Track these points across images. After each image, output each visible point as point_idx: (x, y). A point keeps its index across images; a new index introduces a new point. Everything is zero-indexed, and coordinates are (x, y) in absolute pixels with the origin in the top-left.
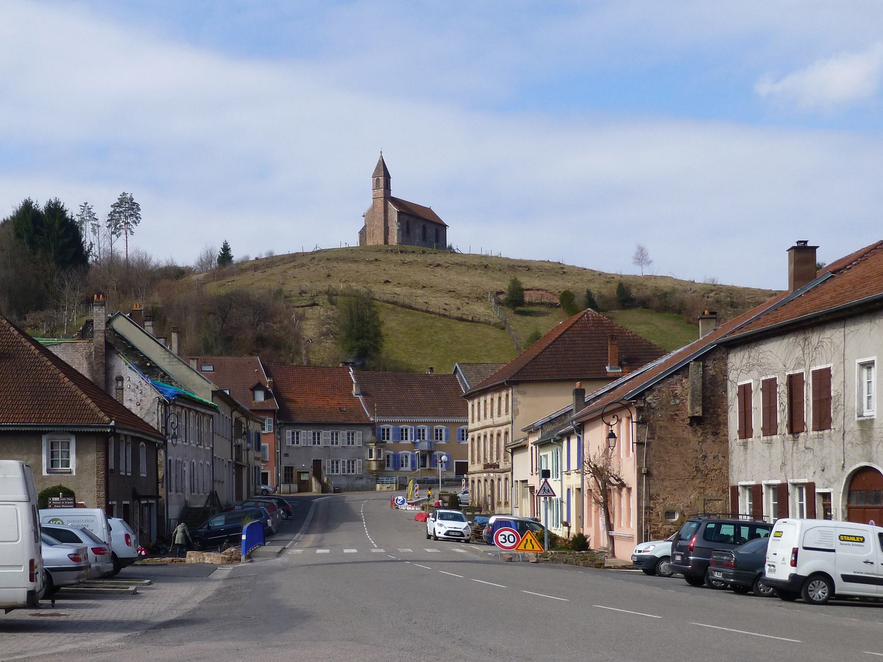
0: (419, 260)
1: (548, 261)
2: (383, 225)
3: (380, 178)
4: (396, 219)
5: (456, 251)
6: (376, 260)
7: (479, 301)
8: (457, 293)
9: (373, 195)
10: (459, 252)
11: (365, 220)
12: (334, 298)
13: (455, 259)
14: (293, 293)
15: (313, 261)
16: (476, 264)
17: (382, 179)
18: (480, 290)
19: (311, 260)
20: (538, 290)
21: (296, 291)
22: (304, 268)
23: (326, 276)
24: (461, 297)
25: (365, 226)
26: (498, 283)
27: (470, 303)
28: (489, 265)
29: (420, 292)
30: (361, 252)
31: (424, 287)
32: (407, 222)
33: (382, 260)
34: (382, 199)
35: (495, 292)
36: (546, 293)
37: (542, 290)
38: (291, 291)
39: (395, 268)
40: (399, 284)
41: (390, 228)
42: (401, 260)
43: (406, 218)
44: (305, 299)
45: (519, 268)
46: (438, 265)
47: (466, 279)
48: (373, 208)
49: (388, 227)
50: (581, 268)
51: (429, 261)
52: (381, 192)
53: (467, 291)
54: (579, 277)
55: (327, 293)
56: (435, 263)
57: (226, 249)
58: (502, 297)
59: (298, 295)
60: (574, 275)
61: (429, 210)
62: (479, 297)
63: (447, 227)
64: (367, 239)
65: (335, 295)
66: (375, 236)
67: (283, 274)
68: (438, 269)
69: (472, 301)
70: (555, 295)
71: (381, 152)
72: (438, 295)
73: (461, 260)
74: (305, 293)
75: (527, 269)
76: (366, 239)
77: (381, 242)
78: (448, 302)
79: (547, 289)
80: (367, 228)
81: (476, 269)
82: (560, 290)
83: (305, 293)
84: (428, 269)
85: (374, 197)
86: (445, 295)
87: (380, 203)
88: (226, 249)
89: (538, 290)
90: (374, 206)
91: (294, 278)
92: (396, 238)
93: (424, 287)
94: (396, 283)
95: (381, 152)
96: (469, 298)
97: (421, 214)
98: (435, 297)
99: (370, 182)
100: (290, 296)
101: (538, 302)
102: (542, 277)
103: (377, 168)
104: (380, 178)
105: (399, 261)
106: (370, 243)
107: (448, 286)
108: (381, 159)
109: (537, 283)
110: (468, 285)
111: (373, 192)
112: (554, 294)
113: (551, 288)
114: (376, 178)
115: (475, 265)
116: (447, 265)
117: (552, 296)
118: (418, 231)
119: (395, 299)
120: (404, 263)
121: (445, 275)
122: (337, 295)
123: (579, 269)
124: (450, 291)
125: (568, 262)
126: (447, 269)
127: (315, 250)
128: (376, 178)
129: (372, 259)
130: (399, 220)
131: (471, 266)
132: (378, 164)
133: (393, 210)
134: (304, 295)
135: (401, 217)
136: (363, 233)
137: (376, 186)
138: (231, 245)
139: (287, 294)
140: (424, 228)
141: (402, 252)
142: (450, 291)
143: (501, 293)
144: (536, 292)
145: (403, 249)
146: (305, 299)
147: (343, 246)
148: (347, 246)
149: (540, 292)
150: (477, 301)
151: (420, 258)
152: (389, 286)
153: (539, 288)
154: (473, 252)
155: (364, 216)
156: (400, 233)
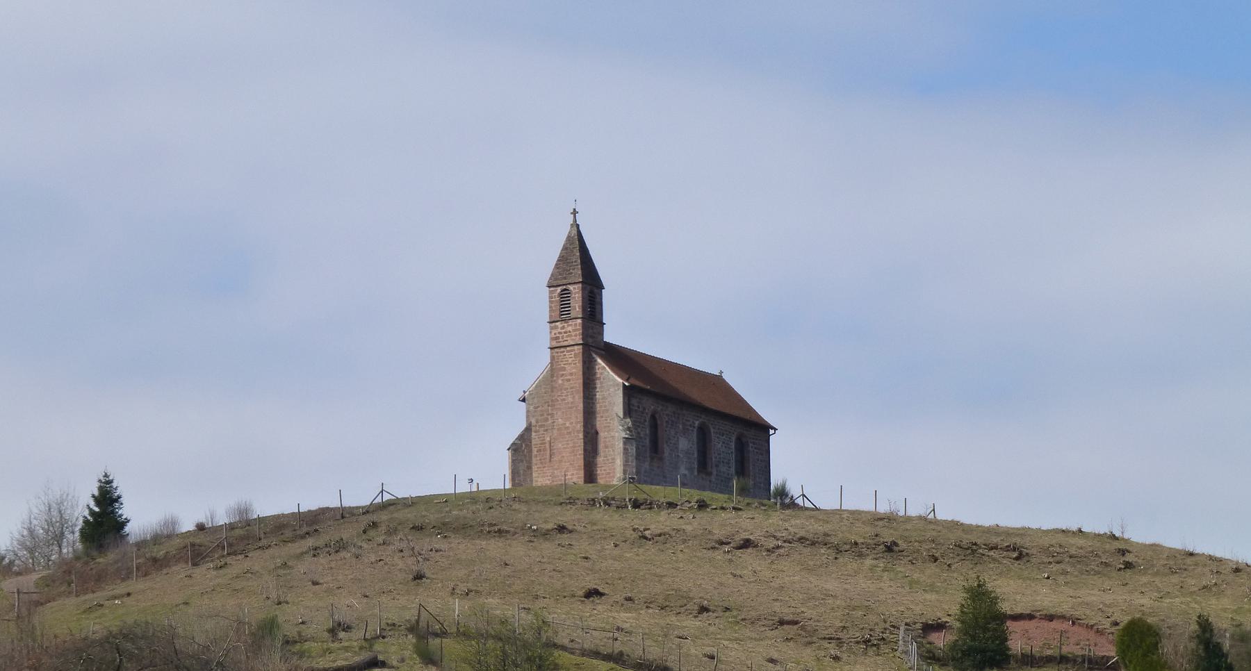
0: (689, 528)
1: (1080, 531)
2: (580, 427)
3: (571, 287)
4: (619, 408)
5: (800, 501)
6: (562, 529)
7: (871, 651)
8: (803, 628)
9: (552, 339)
10: (808, 504)
11: (528, 412)
12: (434, 643)
13: (796, 525)
14: (309, 631)
15: (372, 533)
16: (860, 541)
17: (576, 292)
18: (872, 618)
19: (365, 532)
20: (1051, 618)
21: (318, 625)
22: (343, 554)
23: (411, 577)
24: (814, 639)
25: (528, 429)
26: (928, 596)
27: (844, 656)
28: (900, 542)
29: (691, 624)
30: (516, 506)
31: (703, 609)
32: (653, 417)
33: (578, 528)
34: (578, 349)
35: (919, 626)
36: (1076, 628)
37: (1063, 617)
38: (303, 623)
39: (617, 552)
40: (629, 599)
41: (602, 435)
42: (634, 530)
43: (649, 405)
44: (346, 649)
45: (991, 553)
46: (746, 544)
47: (832, 585)
48: (552, 376)
49: (597, 433)
50: (1178, 551)
51: (719, 533)
52: (573, 330)
53: (834, 622)
54: (1175, 579)
55: (413, 629)
56: (737, 538)
57: (107, 498)
58: (940, 641)
59: (326, 635)
60: (1157, 574)
61: (716, 383)
62: (869, 641)
63: (771, 432)
64: (534, 468)
65: (436, 635)
66: (556, 458)
67: (281, 572)
68: (747, 555)
69: (850, 650)
70: (1100, 632)
71: (575, 212)
72: (747, 632)
73: (814, 528)
74: (347, 628)
75: (1015, 555)
76: (530, 468)
77: (575, 475)
78: (775, 656)
79: (1077, 614)
80: (533, 434)
81: (861, 555)
82: (1117, 617)
83: (347, 628)
84: (718, 555)
85: (555, 344)
86: (770, 633)
87: (573, 362)
88: (107, 498)
89: (1051, 618)
90: (554, 370)
91: (315, 583)
92: (619, 462)
93: (703, 609)
94: (619, 597)
95: (575, 212)
96: (840, 642)
97: (696, 395)
98: (736, 639)
99: (541, 302)
100: (302, 639)
101: (1049, 652)
102: (1061, 579)
103: (563, 260)
104: (571, 287)
105: (629, 533)
106: (541, 478)
107: (777, 607)
108: (575, 232)
109: (1044, 597)
110: (838, 602)
111: (552, 328)
112: (1098, 631)
113: (1088, 612)
114: (559, 289)
115: (856, 543)
116: (772, 543)
117: (1092, 635)
118: (686, 444)
119: (618, 647)
120: (646, 538)
121: (767, 574)
122: (443, 634)
123: (1174, 554)
124: (782, 623)
125: (1139, 533)
126: (774, 556)
127: (379, 500)
128: (559, 289)
129: (550, 526)
130: (628, 411)
131: (847, 547)
132: (565, 248)
133: (611, 382)
134: (342, 635)
135: (634, 401)
136: (521, 450)
137: (561, 311)
138: (122, 487)
139: (292, 632)
140: (703, 436)
141: (636, 505)
142: (782, 623)
143: (939, 627)
144: (1046, 624)
145: (641, 497)
146: (346, 649)
147: (463, 488)
148: (475, 489)
149: (1055, 624)
150: (865, 653)
151: (692, 523)
152: (599, 607)
153: (1052, 611)
154: (852, 503)
155: (524, 400)
156: (633, 450)
